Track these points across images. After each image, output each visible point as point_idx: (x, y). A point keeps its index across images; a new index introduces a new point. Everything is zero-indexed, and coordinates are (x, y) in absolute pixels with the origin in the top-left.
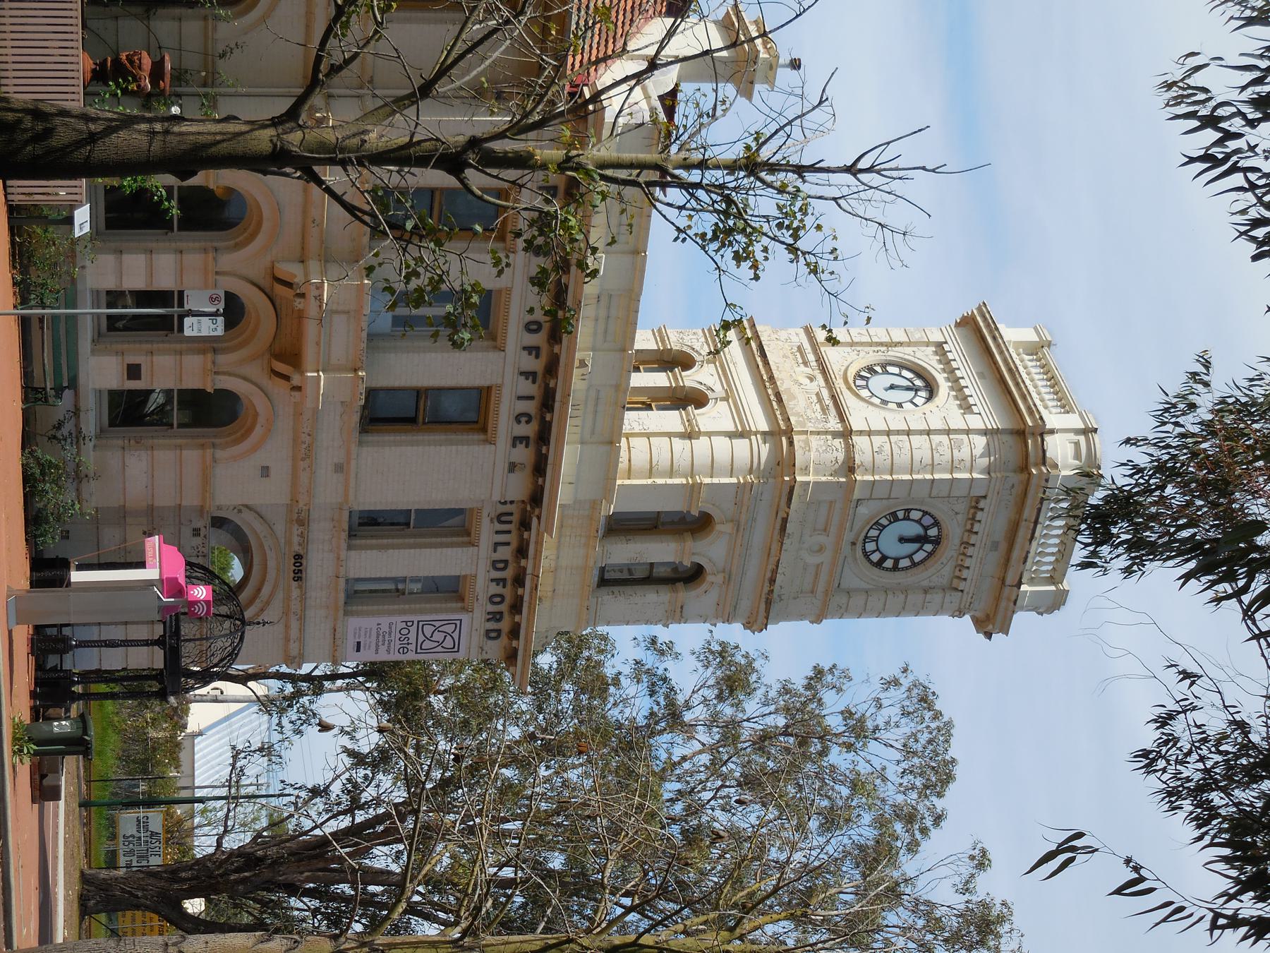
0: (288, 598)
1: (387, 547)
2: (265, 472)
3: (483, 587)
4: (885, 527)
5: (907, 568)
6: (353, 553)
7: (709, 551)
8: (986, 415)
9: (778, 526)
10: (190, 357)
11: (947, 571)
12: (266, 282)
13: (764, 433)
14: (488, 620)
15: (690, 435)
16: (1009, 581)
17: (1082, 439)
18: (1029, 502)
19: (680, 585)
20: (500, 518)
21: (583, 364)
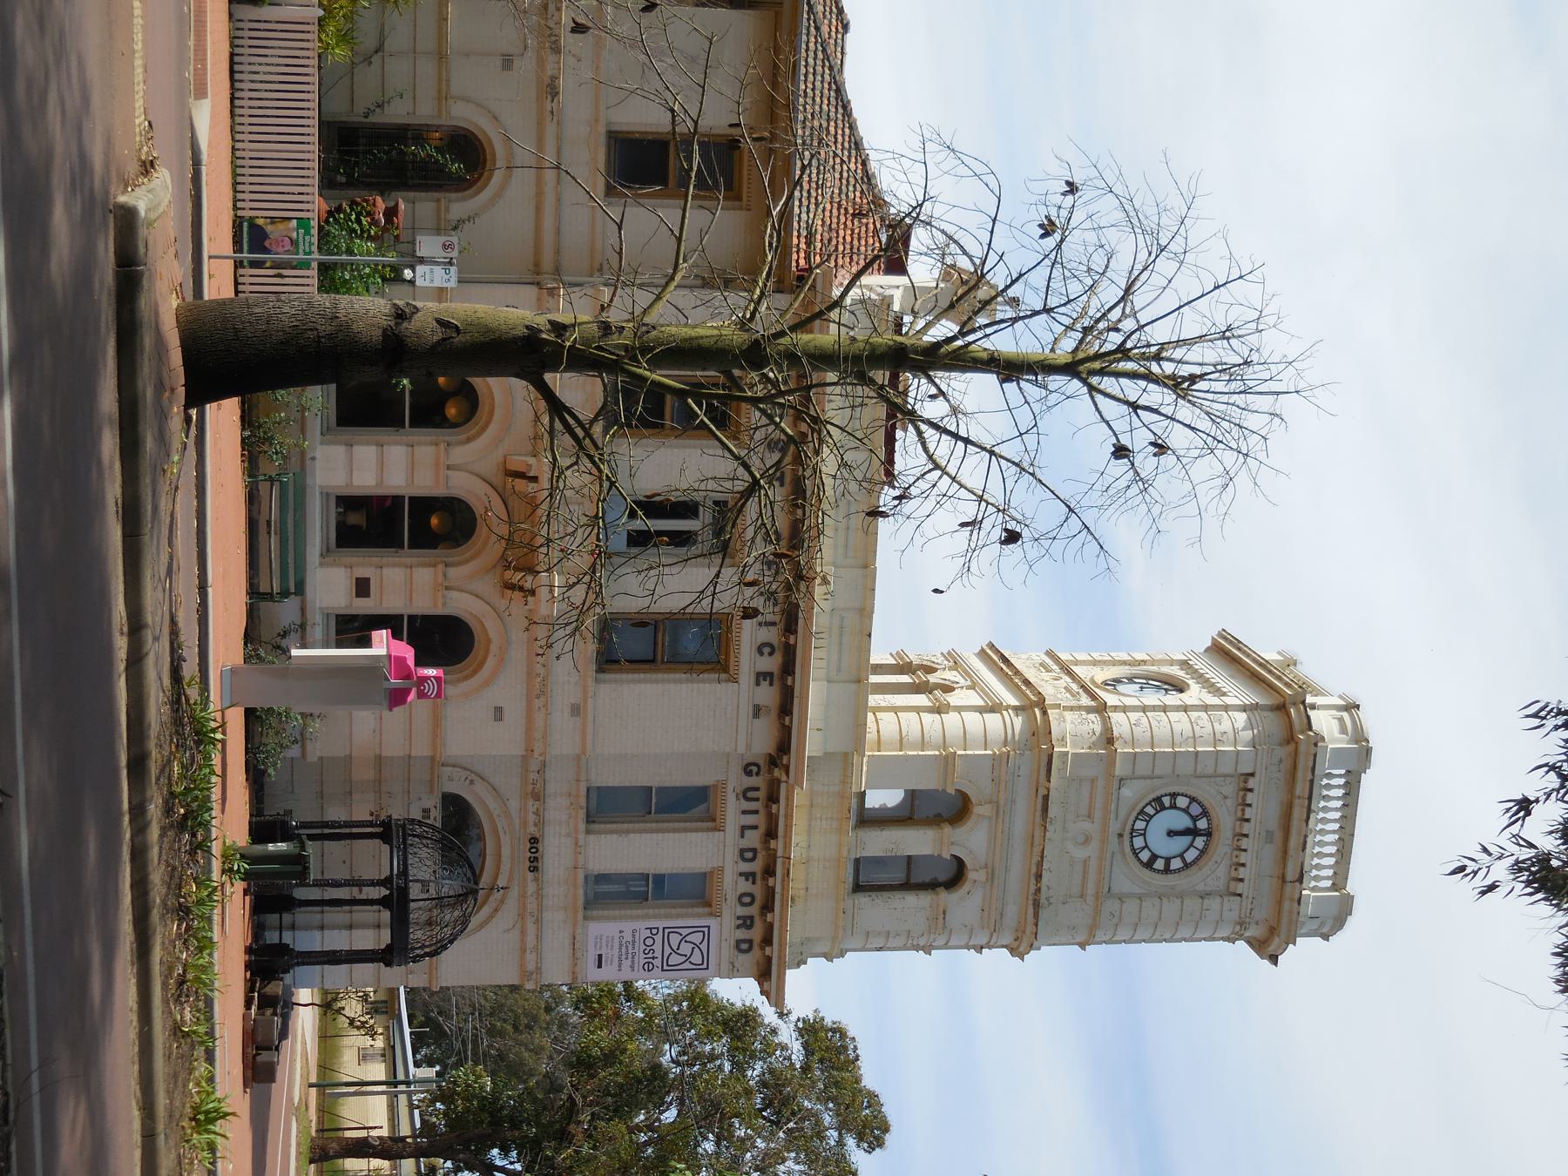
0: (523, 897)
1: (628, 832)
2: (498, 713)
3: (731, 884)
4: (1151, 817)
5: (1179, 870)
6: (592, 838)
7: (970, 841)
8: (1238, 693)
9: (1039, 807)
10: (423, 448)
11: (1222, 870)
12: (498, 479)
13: (1015, 708)
14: (738, 927)
15: (939, 709)
16: (1290, 876)
17: (1345, 715)
18: (1300, 774)
19: (941, 890)
20: (745, 794)
21: (825, 581)
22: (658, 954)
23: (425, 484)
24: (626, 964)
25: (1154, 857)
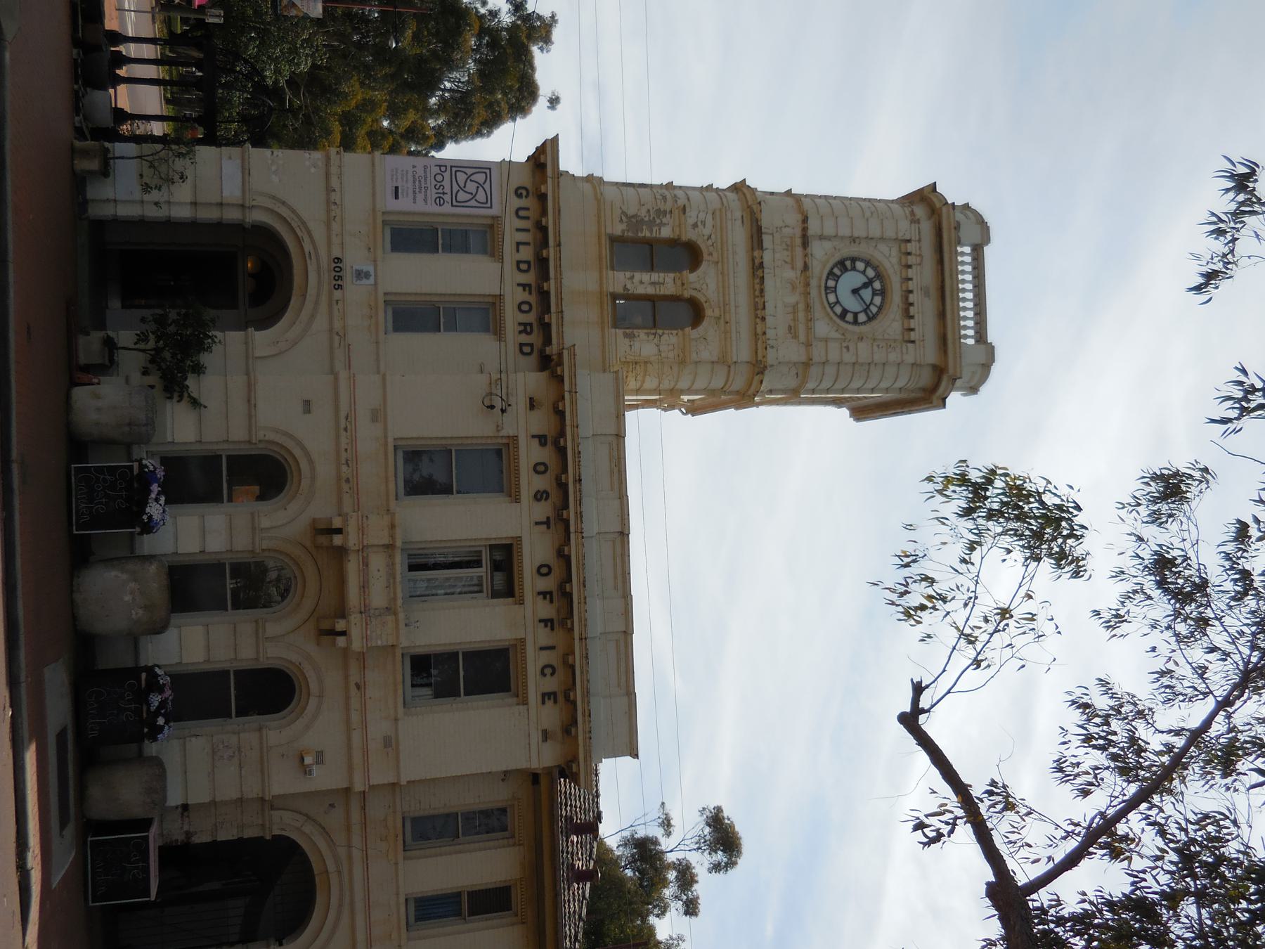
7: (703, 283)
14: (520, 332)
22: (447, 190)
24: (420, 197)
25: (845, 312)
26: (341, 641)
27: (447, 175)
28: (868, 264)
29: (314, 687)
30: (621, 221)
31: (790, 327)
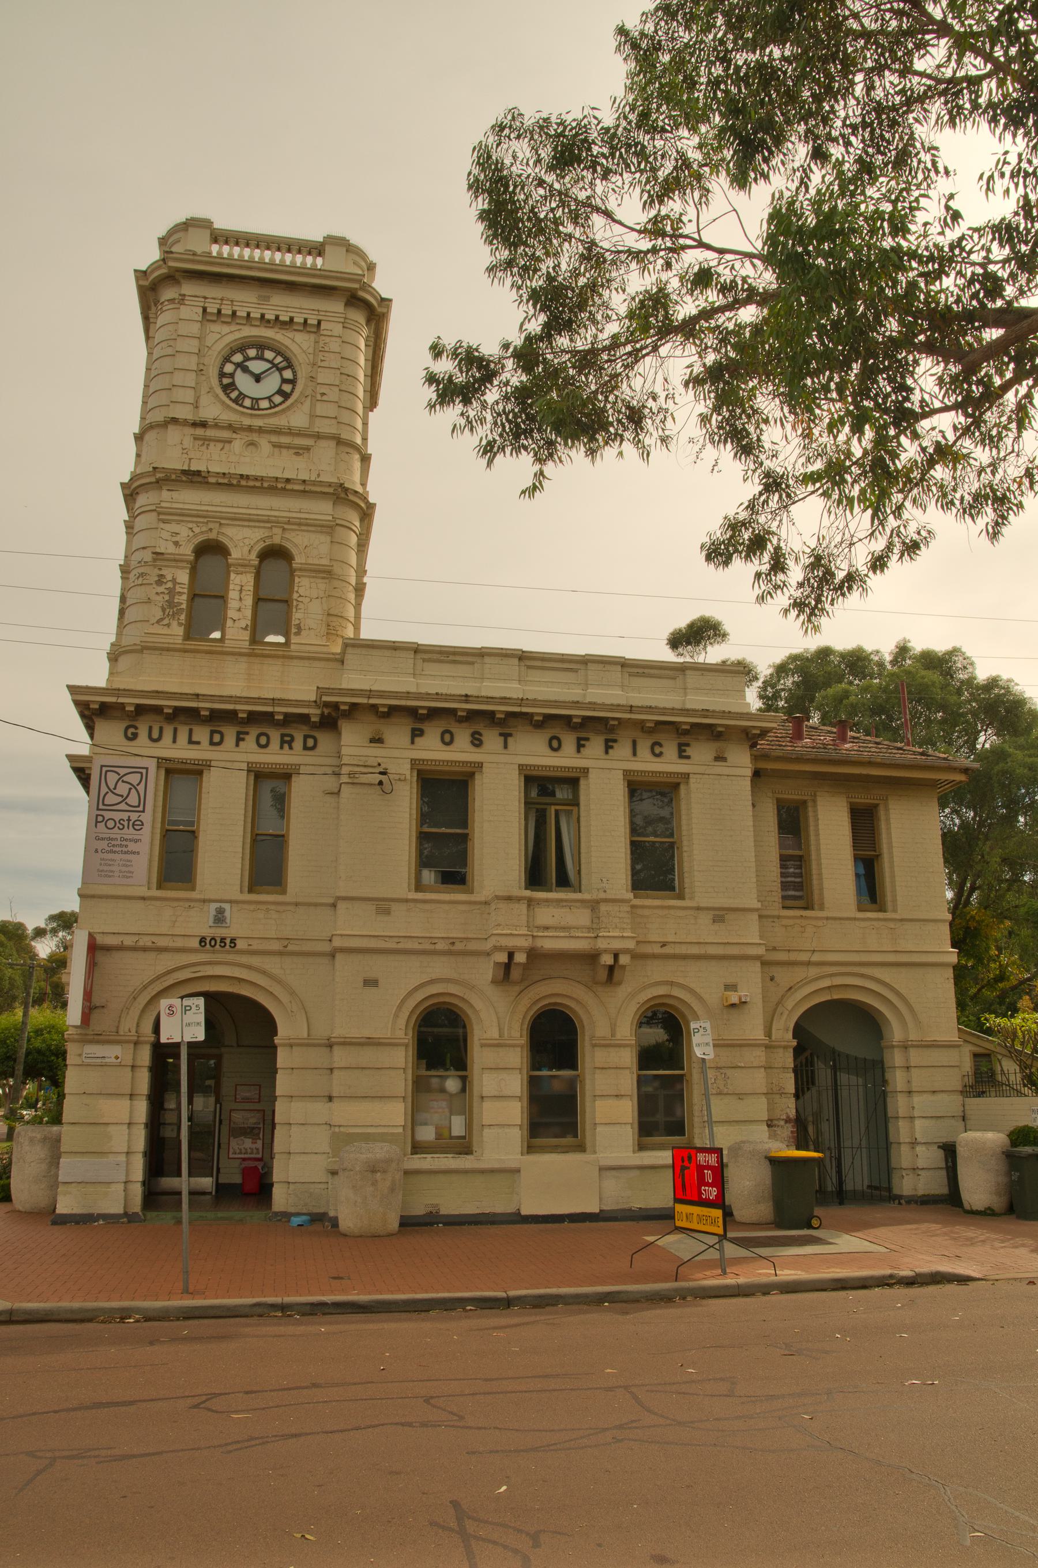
7: (243, 543)
11: (300, 337)
14: (291, 748)
23: (517, 1057)
24: (132, 847)
26: (624, 960)
27: (108, 815)
28: (227, 360)
29: (661, 991)
30: (168, 625)
31: (297, 454)
